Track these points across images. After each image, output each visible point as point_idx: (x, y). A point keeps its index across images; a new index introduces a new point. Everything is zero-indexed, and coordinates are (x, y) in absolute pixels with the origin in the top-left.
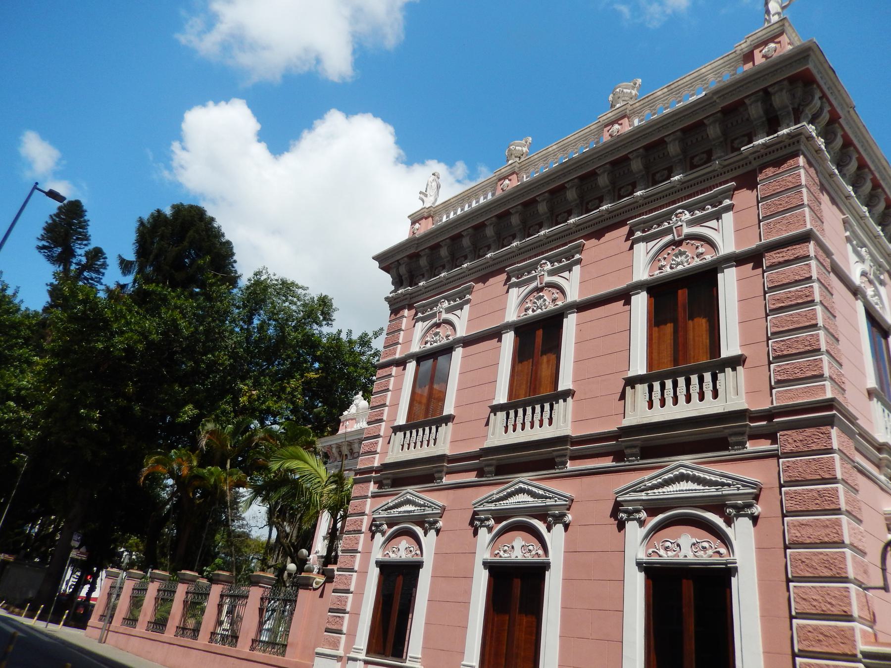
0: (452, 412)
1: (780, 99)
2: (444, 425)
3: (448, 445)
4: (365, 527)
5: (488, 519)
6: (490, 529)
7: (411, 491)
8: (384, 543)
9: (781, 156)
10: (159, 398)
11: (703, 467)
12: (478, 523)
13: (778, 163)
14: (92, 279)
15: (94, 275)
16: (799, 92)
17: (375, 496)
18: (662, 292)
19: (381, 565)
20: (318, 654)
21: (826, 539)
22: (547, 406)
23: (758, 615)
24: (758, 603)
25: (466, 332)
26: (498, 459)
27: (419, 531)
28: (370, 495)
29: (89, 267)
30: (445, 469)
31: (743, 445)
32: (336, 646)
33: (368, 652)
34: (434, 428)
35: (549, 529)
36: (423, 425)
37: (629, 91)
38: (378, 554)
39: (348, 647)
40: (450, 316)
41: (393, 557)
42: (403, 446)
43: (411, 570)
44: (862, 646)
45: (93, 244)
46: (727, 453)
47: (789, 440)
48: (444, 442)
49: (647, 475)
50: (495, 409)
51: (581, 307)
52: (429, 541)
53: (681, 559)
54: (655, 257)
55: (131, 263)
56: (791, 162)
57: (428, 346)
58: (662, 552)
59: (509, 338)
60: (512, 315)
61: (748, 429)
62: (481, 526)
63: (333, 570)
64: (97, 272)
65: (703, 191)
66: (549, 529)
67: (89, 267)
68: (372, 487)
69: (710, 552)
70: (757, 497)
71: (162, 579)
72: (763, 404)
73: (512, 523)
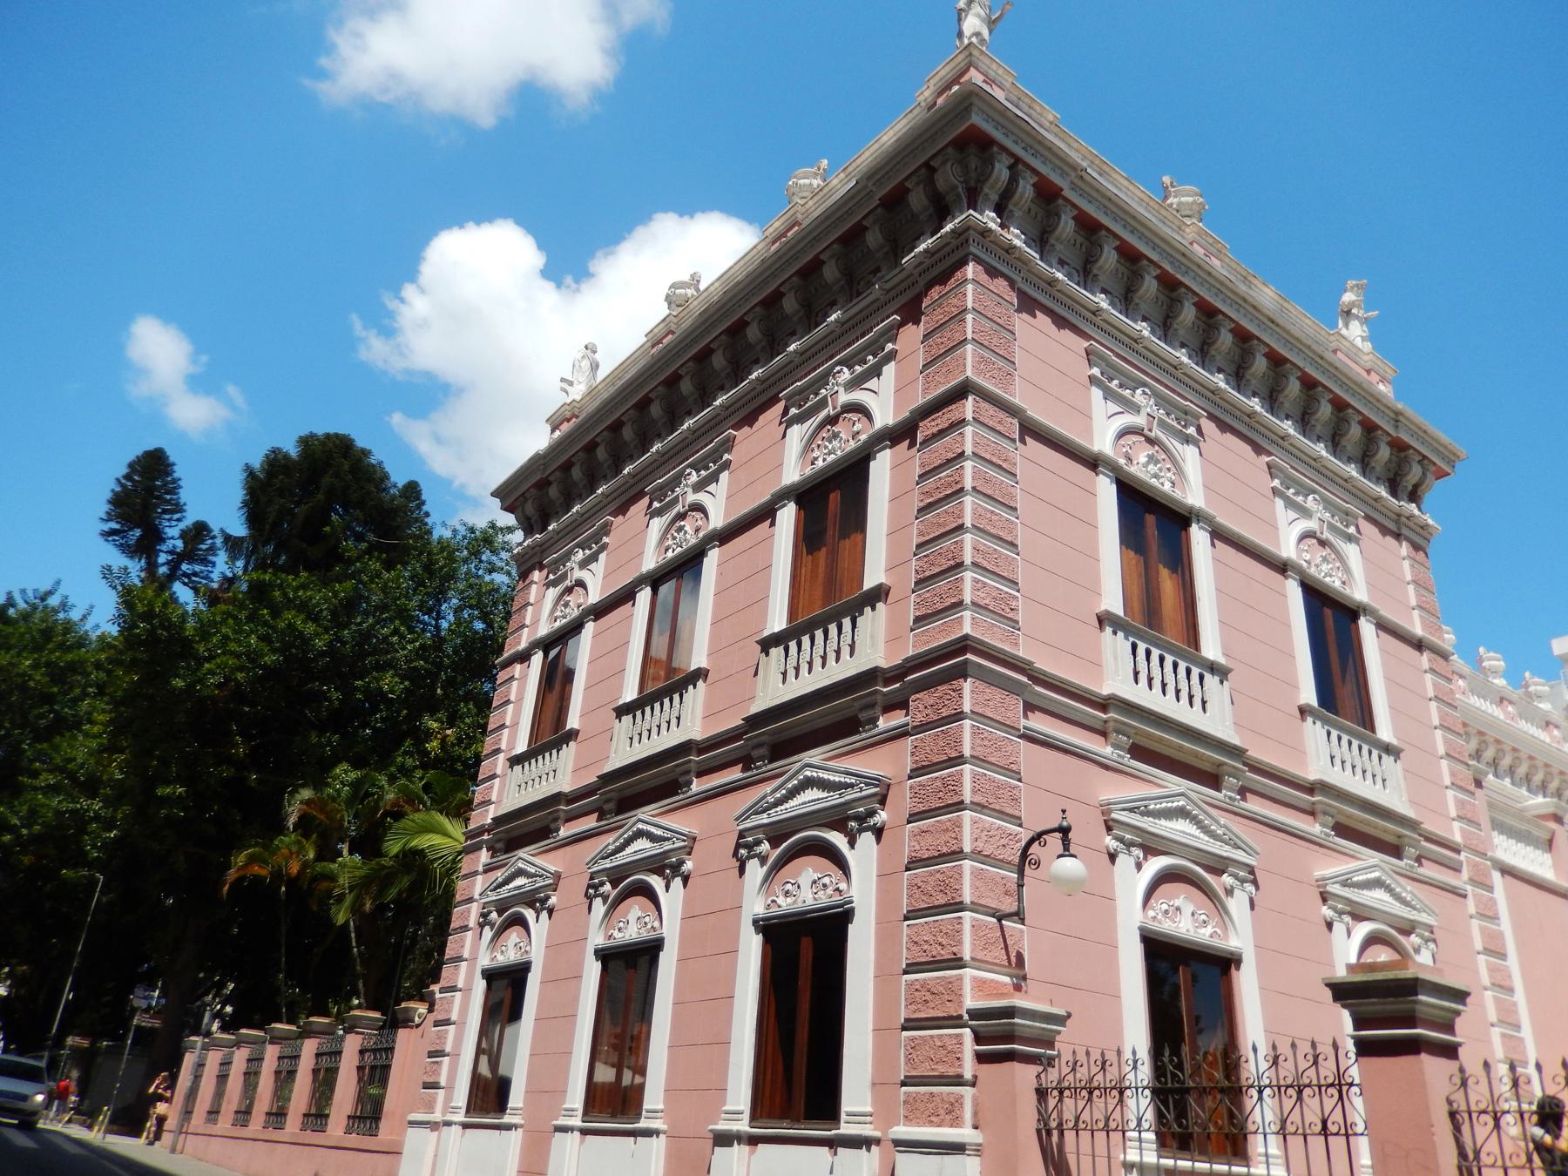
0: (704, 665)
1: (949, 177)
2: (868, 609)
3: (881, 646)
4: (472, 923)
5: (758, 843)
6: (763, 859)
7: (814, 761)
8: (765, 880)
9: (944, 268)
10: (267, 755)
11: (831, 764)
12: (743, 852)
13: (943, 278)
14: (195, 574)
15: (197, 568)
16: (973, 163)
17: (489, 869)
18: (809, 496)
19: (604, 955)
20: (412, 1123)
21: (945, 850)
22: (847, 622)
23: (871, 975)
24: (872, 956)
25: (895, 415)
26: (620, 789)
27: (837, 839)
28: (481, 869)
29: (189, 555)
30: (562, 815)
31: (873, 721)
32: (430, 1107)
33: (755, 1116)
34: (847, 622)
35: (852, 844)
36: (822, 622)
37: (807, 181)
38: (756, 906)
39: (448, 1107)
40: (858, 396)
41: (785, 904)
42: (784, 674)
43: (828, 929)
44: (970, 1002)
45: (190, 519)
46: (857, 737)
47: (923, 705)
48: (694, 718)
49: (768, 788)
50: (767, 644)
51: (724, 536)
52: (672, 897)
53: (799, 906)
54: (808, 447)
55: (241, 539)
56: (958, 274)
57: (670, 554)
58: (781, 900)
59: (788, 515)
60: (792, 473)
61: (879, 697)
62: (750, 857)
63: (433, 993)
64: (204, 561)
65: (863, 335)
66: (852, 844)
67: (189, 555)
68: (484, 856)
69: (830, 891)
70: (883, 802)
71: (370, 1024)
72: (911, 648)
73: (796, 843)
